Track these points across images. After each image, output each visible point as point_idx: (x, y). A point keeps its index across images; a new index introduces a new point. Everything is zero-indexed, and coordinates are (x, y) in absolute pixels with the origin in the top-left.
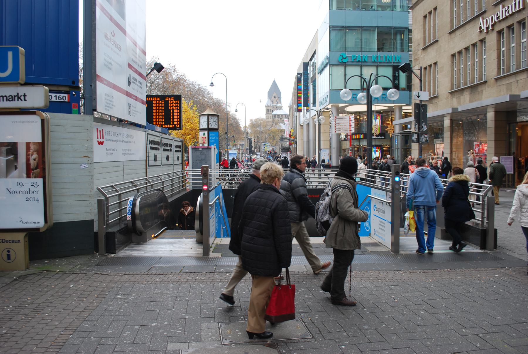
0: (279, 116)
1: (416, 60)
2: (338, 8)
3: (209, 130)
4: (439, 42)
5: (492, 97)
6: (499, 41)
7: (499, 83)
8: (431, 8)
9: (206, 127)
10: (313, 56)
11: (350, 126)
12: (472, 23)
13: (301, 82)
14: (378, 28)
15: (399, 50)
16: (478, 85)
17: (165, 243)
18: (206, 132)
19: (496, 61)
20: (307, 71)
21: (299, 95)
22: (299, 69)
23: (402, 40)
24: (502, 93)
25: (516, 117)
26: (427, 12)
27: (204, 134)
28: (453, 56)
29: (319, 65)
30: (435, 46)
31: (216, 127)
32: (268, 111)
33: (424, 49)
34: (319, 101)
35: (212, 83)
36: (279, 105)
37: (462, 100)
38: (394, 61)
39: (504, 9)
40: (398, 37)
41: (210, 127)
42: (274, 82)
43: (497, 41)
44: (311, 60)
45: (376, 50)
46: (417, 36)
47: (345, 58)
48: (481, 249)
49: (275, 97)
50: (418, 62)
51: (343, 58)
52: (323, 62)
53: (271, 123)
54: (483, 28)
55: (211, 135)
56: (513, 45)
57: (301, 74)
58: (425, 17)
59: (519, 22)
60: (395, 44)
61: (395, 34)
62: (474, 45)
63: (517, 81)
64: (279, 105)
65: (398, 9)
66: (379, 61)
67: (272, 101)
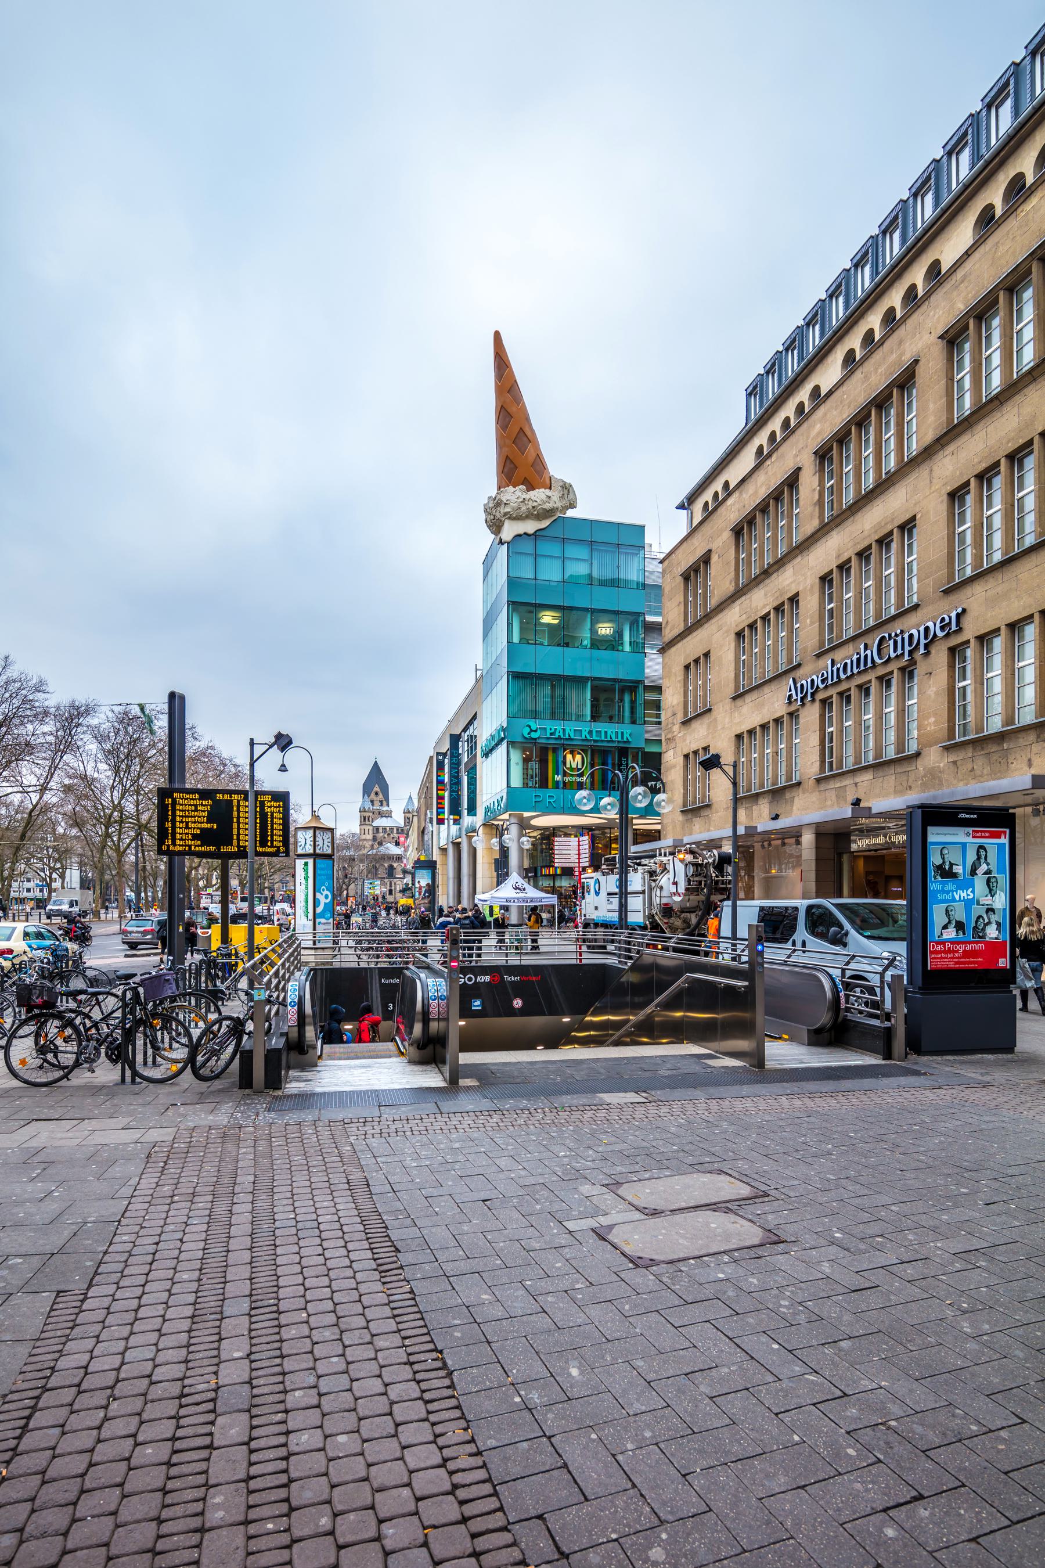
0: (384, 829)
1: (669, 740)
2: (523, 640)
3: (315, 856)
4: (714, 713)
5: (809, 810)
6: (822, 716)
7: (823, 787)
8: (699, 652)
9: (311, 851)
10: (471, 723)
11: (579, 854)
12: (776, 682)
13: (443, 769)
14: (593, 679)
15: (627, 719)
16: (784, 788)
17: (351, 1067)
18: (311, 862)
19: (818, 748)
20: (458, 749)
21: (441, 793)
22: (438, 743)
23: (633, 703)
24: (829, 803)
25: (849, 842)
26: (690, 660)
27: (306, 864)
28: (739, 737)
29: (482, 742)
30: (706, 720)
31: (329, 852)
32: (364, 820)
33: (684, 723)
34: (485, 805)
35: (283, 765)
36: (385, 808)
37: (755, 813)
38: (620, 739)
39: (835, 669)
40: (627, 698)
41: (318, 851)
42: (376, 767)
43: (820, 715)
44: (465, 730)
45: (589, 718)
46: (672, 699)
47: (536, 731)
48: (884, 1059)
49: (377, 794)
50: (673, 745)
51: (532, 731)
52: (493, 737)
53: (370, 843)
54: (795, 697)
55: (318, 866)
56: (850, 723)
57: (444, 755)
58: (687, 667)
59: (859, 687)
60: (621, 709)
61: (622, 691)
62: (778, 721)
63: (856, 784)
64: (385, 808)
65: (627, 648)
66: (594, 738)
67: (372, 802)
